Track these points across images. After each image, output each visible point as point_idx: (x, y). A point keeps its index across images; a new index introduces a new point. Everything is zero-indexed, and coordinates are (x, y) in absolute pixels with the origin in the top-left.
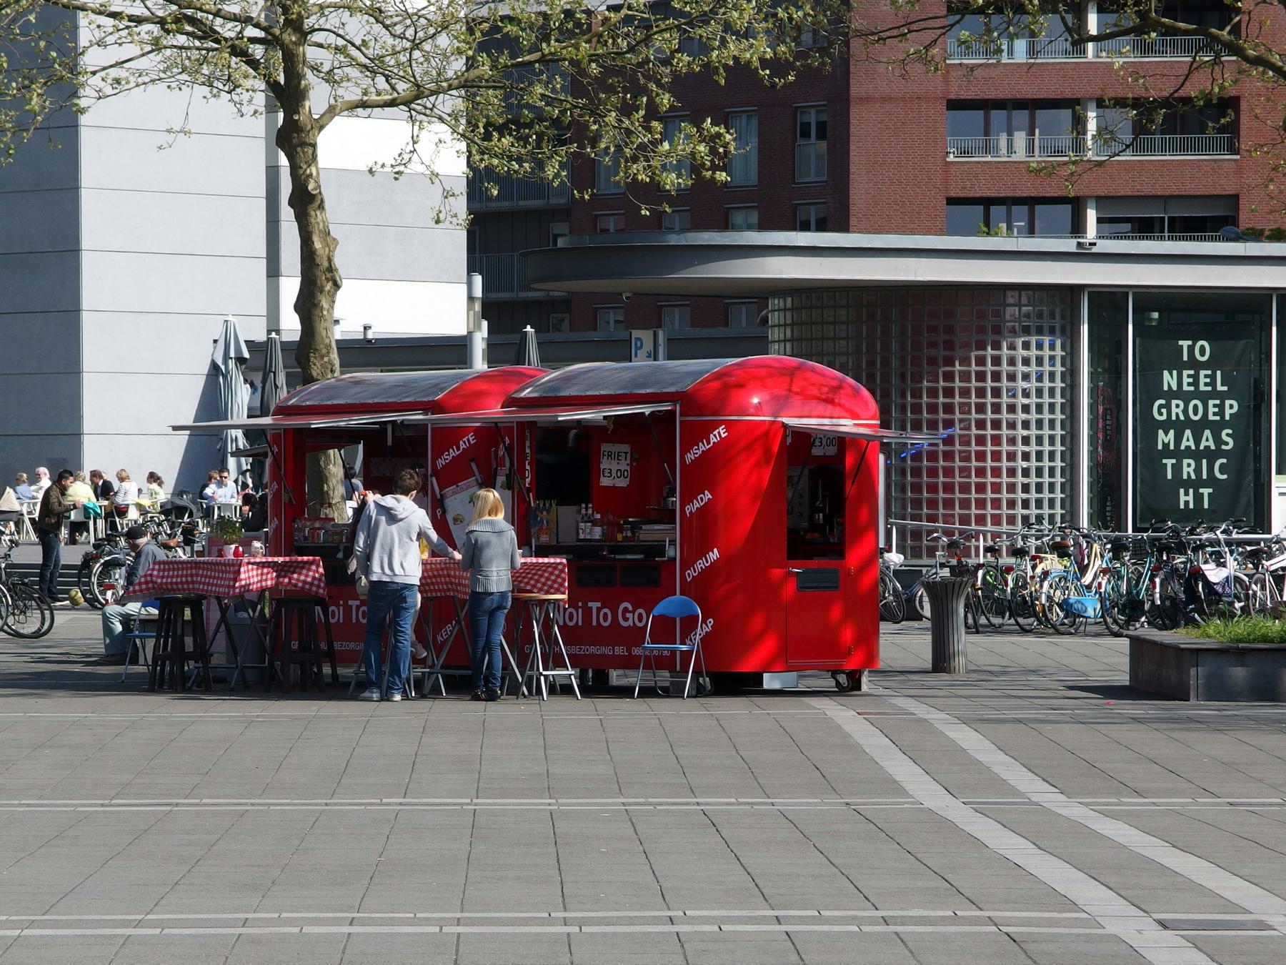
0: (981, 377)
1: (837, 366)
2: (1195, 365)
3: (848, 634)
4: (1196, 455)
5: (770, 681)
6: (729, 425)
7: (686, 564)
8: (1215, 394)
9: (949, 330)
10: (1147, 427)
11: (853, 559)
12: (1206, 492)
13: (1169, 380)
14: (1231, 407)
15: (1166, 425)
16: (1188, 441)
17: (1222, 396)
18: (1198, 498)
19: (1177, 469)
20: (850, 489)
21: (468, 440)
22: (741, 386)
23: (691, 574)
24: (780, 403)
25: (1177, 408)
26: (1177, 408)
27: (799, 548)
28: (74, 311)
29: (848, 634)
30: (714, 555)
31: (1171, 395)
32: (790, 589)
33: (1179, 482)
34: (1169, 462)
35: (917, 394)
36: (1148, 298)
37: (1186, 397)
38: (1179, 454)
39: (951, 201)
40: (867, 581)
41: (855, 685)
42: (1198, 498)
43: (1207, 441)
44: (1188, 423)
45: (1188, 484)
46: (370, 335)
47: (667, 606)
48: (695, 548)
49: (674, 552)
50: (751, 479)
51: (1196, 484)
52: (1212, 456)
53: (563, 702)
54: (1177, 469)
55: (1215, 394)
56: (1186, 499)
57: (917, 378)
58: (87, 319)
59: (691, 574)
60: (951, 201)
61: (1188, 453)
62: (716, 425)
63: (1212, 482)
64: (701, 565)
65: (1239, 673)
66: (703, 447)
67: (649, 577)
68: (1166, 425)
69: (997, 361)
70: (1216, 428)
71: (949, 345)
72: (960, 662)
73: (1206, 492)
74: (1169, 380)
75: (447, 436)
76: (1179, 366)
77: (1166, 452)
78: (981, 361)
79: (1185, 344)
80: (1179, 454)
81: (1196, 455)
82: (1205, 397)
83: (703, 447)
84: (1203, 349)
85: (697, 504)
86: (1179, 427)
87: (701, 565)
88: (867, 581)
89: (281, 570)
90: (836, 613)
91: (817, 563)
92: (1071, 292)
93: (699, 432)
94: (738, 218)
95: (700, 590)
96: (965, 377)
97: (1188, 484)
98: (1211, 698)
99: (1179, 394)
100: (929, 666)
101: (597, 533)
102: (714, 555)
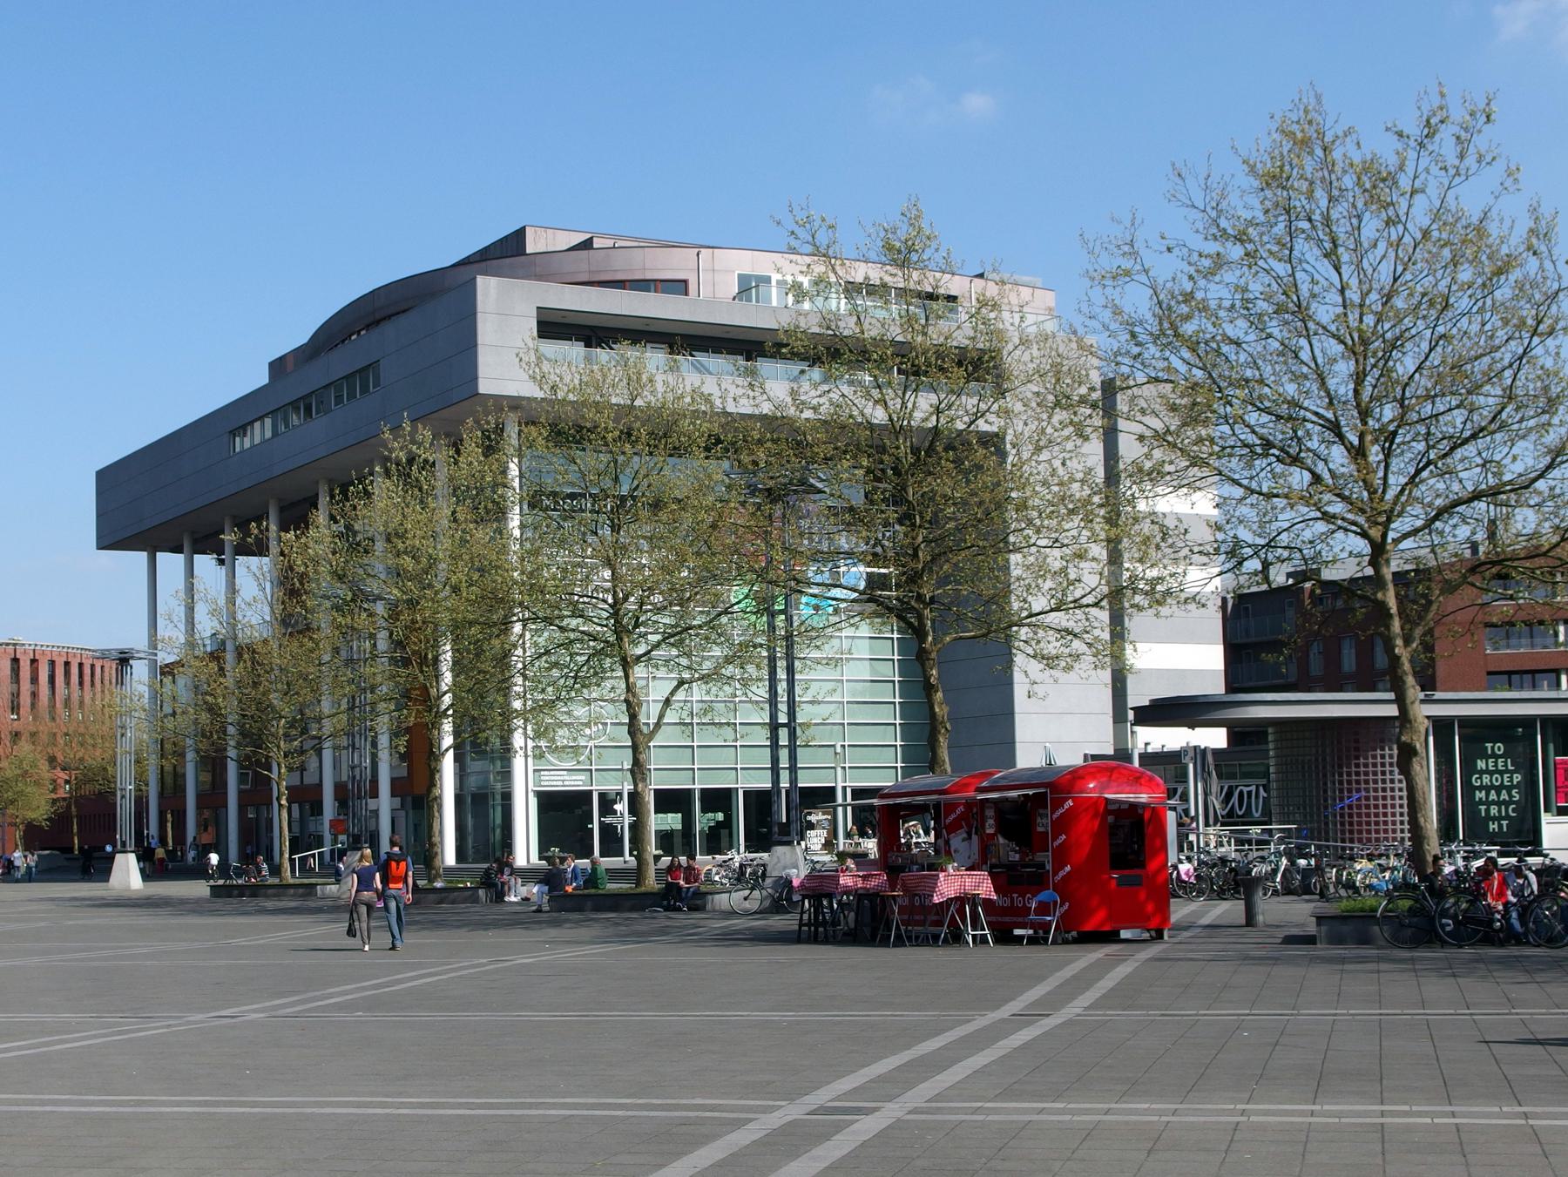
0: (1375, 765)
1: (473, 782)
2: (1496, 757)
3: (1150, 907)
4: (1498, 803)
5: (1124, 934)
6: (1074, 799)
7: (1055, 873)
8: (1507, 771)
9: (1357, 741)
10: (1469, 789)
11: (1153, 866)
12: (1505, 823)
13: (1481, 764)
14: (1517, 778)
15: (1481, 788)
16: (1493, 796)
17: (1512, 772)
18: (1500, 826)
19: (1487, 811)
20: (1149, 830)
21: (962, 808)
22: (1082, 778)
23: (1058, 878)
24: (1103, 789)
25: (1486, 779)
26: (1486, 779)
27: (1118, 862)
28: (1012, 743)
29: (1150, 907)
30: (1068, 868)
31: (1482, 772)
32: (1114, 883)
33: (1489, 818)
34: (1483, 808)
35: (1341, 775)
36: (1465, 722)
37: (1491, 773)
38: (1488, 803)
39: (1489, 673)
40: (1160, 879)
41: (1160, 936)
42: (1500, 826)
43: (1504, 796)
44: (1492, 787)
45: (1494, 819)
46: (1150, 750)
47: (1044, 896)
48: (1058, 867)
49: (1049, 867)
50: (1087, 827)
51: (1499, 819)
52: (1507, 804)
53: (982, 949)
54: (1487, 811)
55: (1507, 771)
56: (1493, 826)
57: (1340, 767)
58: (1018, 746)
59: (1058, 878)
60: (1489, 673)
61: (1493, 802)
62: (1066, 799)
63: (1507, 817)
64: (1061, 874)
65: (1346, 928)
66: (1061, 811)
67: (1038, 881)
68: (1481, 788)
69: (1383, 757)
70: (1509, 789)
71: (1357, 749)
72: (1260, 918)
73: (1505, 823)
74: (1481, 764)
75: (951, 807)
76: (1486, 757)
77: (1481, 802)
78: (1374, 757)
79: (1489, 745)
80: (1488, 803)
81: (1498, 803)
82: (1501, 773)
83: (1061, 811)
84: (1500, 748)
85: (1059, 842)
86: (1488, 789)
87: (1061, 874)
88: (1160, 879)
89: (864, 878)
90: (1143, 895)
91: (1126, 872)
92: (1528, 722)
93: (1058, 803)
94: (1380, 685)
95: (1062, 888)
96: (1366, 765)
97: (1494, 819)
98: (1330, 943)
99: (1487, 771)
100: (1243, 922)
101: (1017, 857)
102: (1068, 868)
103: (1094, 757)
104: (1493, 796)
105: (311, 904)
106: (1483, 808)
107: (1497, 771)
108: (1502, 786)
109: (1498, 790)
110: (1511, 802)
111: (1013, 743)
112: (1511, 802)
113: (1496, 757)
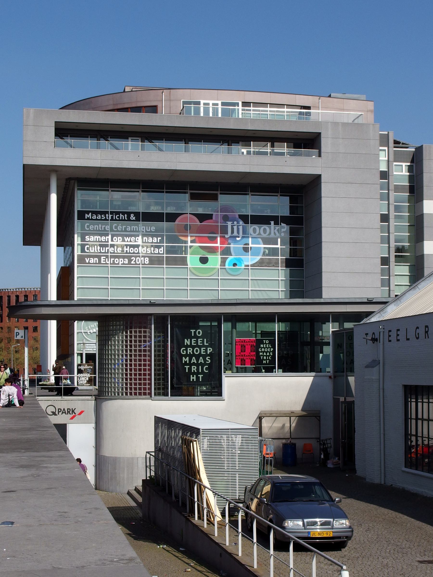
8: (269, 348)
12: (268, 361)
14: (272, 349)
16: (265, 354)
17: (271, 348)
18: (198, 378)
33: (190, 373)
34: (187, 367)
38: (191, 365)
42: (198, 378)
43: (268, 354)
44: (265, 352)
45: (265, 360)
52: (203, 365)
61: (265, 356)
63: (269, 359)
70: (204, 357)
73: (201, 376)
74: (262, 346)
77: (186, 363)
79: (193, 331)
82: (268, 348)
86: (263, 352)
97: (194, 374)
99: (263, 348)
103: (246, 194)
104: (265, 354)
105: (378, 339)
106: (262, 357)
107: (266, 348)
108: (268, 351)
109: (266, 353)
110: (270, 356)
111: (321, 287)
112: (205, 364)
113: (197, 338)
